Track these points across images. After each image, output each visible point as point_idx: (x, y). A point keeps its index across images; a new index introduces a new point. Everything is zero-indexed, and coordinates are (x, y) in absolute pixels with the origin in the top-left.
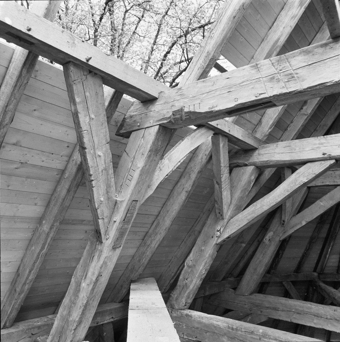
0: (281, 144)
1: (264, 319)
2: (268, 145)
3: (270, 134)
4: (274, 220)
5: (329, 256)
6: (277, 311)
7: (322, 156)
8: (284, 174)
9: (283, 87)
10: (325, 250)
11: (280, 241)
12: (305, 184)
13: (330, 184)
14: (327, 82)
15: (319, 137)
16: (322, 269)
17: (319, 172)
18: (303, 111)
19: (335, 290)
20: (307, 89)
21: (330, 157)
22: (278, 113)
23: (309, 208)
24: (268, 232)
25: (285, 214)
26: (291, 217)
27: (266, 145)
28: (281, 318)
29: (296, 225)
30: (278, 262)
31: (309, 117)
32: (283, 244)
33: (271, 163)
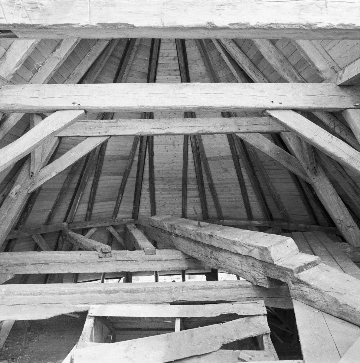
0: (29, 87)
1: (10, 277)
2: (13, 85)
3: (16, 73)
4: (21, 172)
5: (78, 206)
6: (25, 267)
7: (73, 105)
8: (33, 122)
9: (25, 17)
10: (75, 200)
11: (29, 194)
12: (54, 133)
13: (80, 135)
14: (74, 24)
15: (69, 85)
16: (72, 219)
17: (68, 122)
18: (55, 54)
19: (82, 236)
20: (53, 26)
21: (80, 107)
22: (27, 50)
23: (60, 158)
24: (14, 185)
25: (34, 164)
26: (40, 168)
27: (11, 86)
28: (28, 273)
29: (45, 177)
30: (28, 216)
31: (62, 62)
32: (32, 198)
33: (17, 108)
